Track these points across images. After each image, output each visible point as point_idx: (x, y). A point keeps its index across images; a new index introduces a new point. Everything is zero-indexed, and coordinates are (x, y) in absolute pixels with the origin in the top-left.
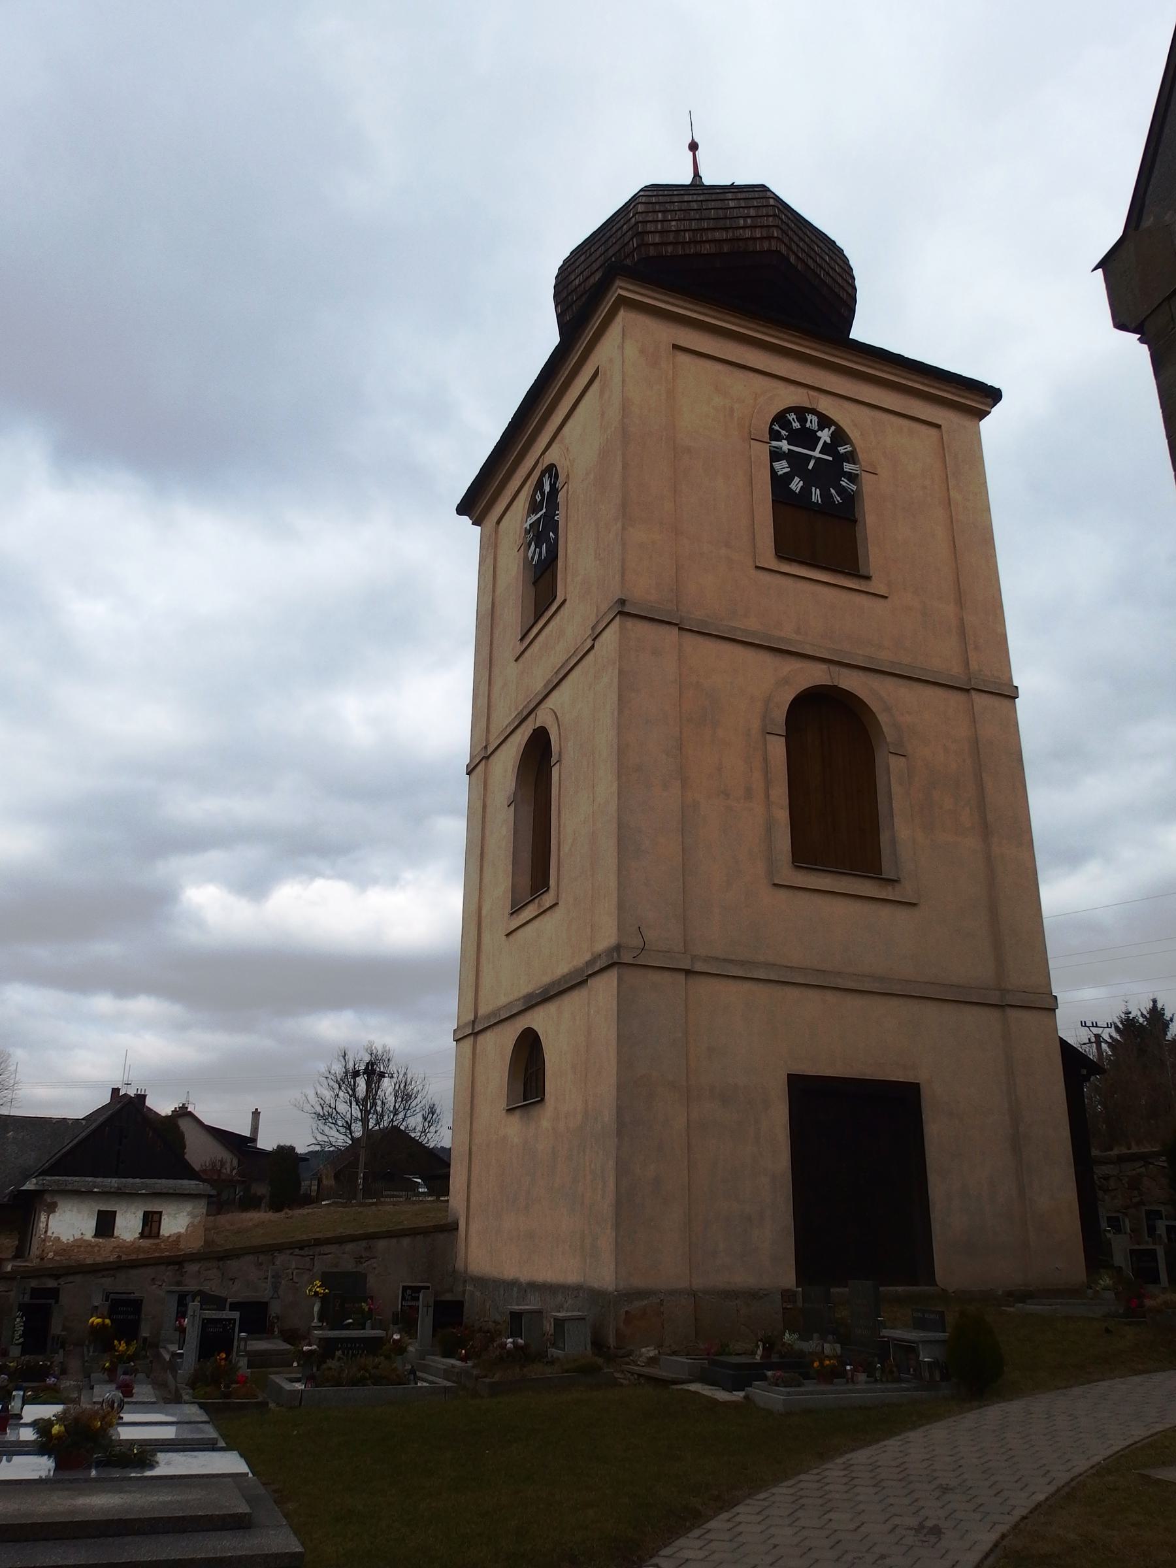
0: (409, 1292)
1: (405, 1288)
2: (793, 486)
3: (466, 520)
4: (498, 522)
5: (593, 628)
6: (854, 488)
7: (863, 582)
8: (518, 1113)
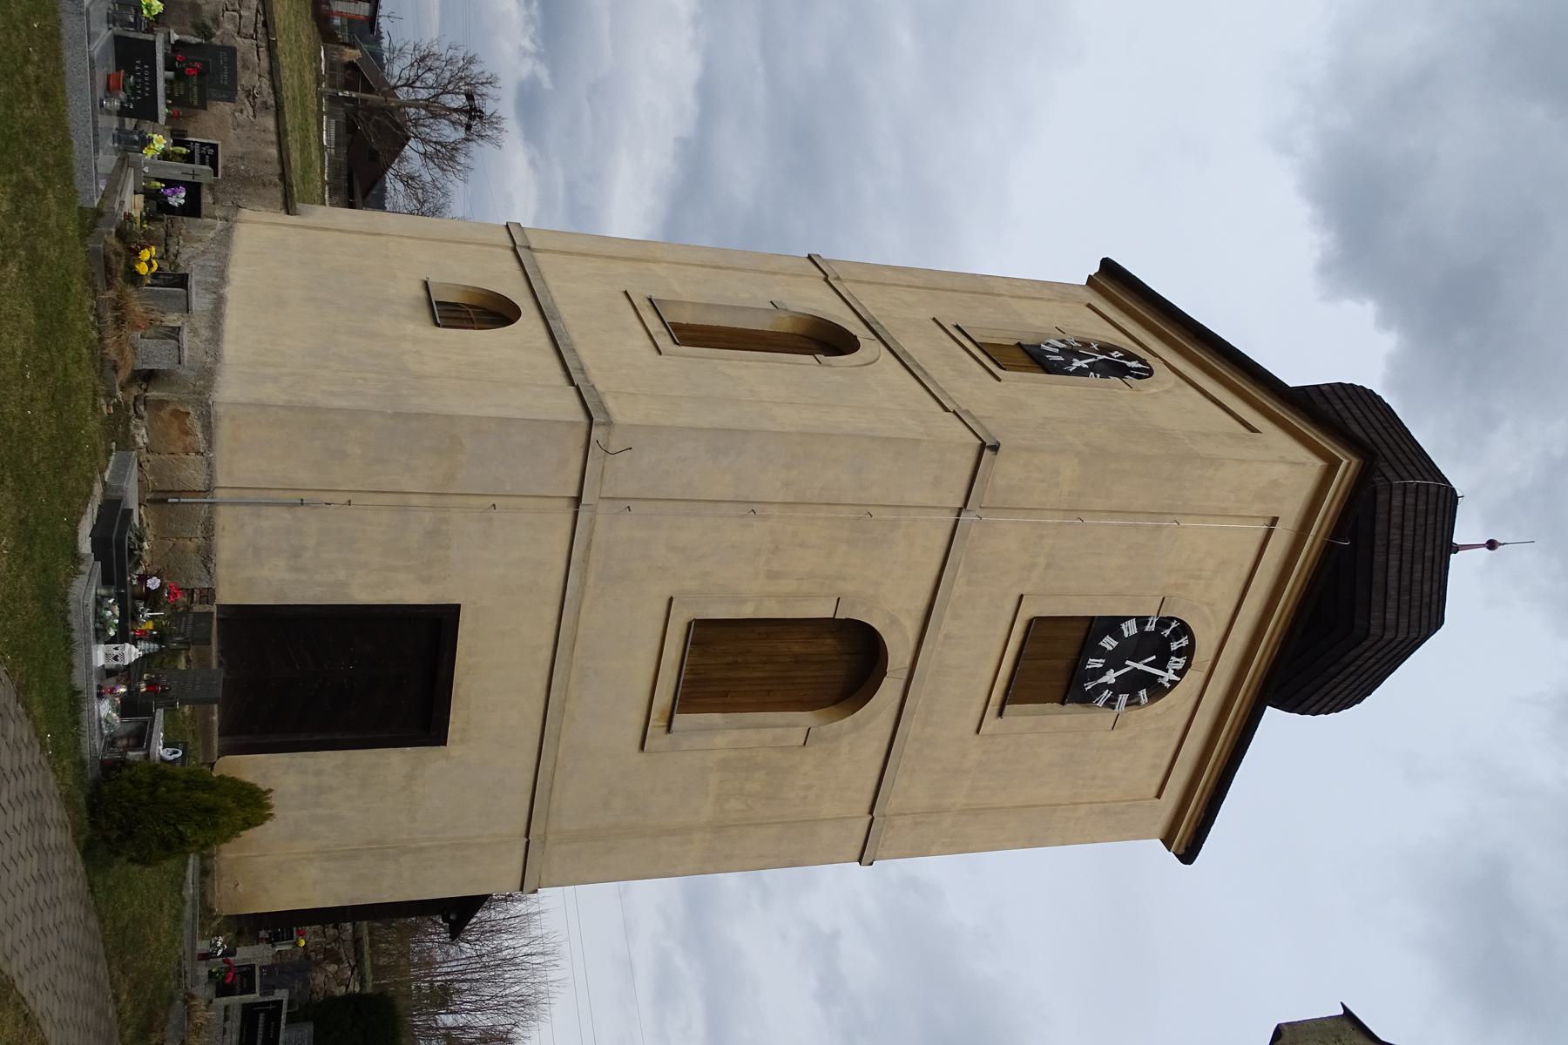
0: (211, 151)
1: (215, 147)
2: (1108, 639)
3: (1095, 268)
4: (1089, 306)
5: (967, 412)
6: (1100, 704)
7: (997, 708)
8: (423, 293)
